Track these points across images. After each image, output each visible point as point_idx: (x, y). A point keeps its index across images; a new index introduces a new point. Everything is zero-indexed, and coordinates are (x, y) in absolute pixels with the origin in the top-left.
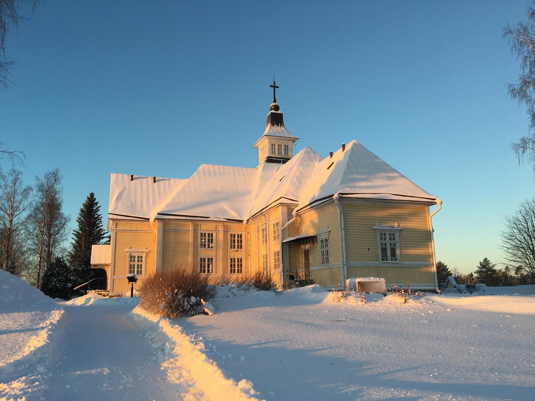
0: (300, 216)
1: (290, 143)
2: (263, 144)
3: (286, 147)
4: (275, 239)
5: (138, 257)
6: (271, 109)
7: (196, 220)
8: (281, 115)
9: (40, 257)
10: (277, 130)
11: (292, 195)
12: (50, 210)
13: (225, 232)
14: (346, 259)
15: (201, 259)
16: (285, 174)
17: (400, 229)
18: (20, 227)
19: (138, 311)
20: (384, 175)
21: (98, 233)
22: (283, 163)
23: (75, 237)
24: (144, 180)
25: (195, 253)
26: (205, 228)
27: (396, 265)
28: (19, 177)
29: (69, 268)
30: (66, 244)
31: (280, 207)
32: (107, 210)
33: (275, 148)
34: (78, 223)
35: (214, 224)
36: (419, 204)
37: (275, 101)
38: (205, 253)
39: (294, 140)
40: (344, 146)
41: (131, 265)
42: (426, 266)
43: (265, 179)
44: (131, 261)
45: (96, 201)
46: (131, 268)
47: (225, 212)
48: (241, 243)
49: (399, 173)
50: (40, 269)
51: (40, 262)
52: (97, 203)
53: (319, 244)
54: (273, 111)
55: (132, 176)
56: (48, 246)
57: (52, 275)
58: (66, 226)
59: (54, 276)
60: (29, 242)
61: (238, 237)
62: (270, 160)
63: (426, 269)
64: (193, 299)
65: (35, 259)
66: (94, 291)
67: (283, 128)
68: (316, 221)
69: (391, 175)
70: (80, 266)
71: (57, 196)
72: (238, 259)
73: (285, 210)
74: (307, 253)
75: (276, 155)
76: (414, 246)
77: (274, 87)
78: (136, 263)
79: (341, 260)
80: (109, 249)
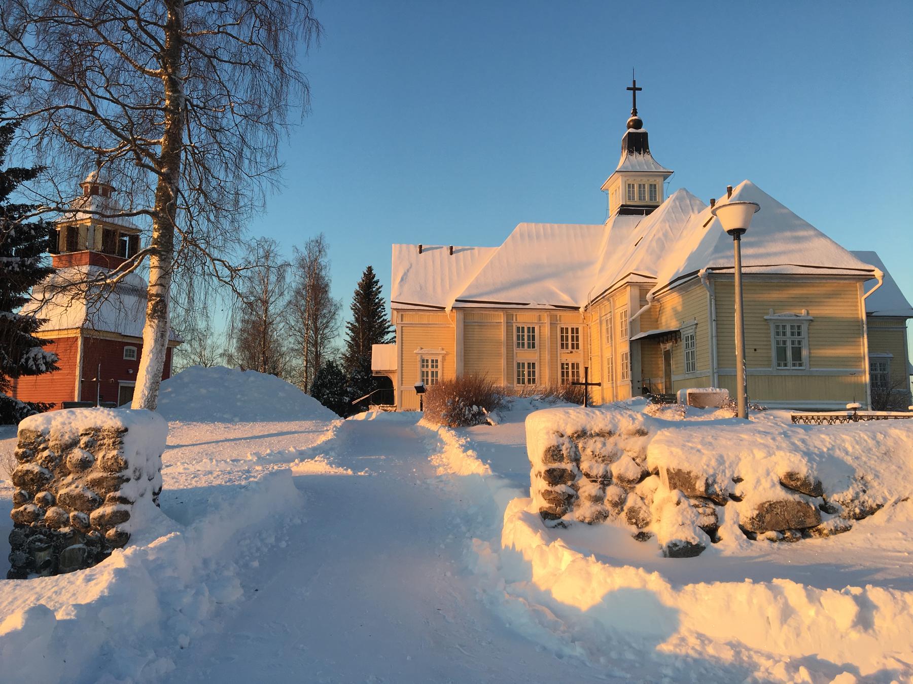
0: (658, 300)
1: (659, 181)
2: (615, 184)
3: (653, 187)
4: (622, 336)
5: (433, 361)
6: (629, 128)
7: (509, 309)
8: (645, 135)
9: (306, 361)
10: (638, 159)
11: (648, 269)
12: (316, 292)
13: (553, 325)
14: (718, 364)
15: (519, 364)
16: (643, 235)
17: (810, 318)
18: (278, 319)
19: (423, 423)
20: (788, 234)
21: (380, 326)
22: (647, 214)
23: (349, 332)
24: (437, 252)
25: (510, 357)
26: (523, 319)
27: (800, 373)
28: (272, 248)
29: (345, 376)
30: (338, 343)
31: (628, 288)
32: (391, 294)
33: (633, 191)
34: (352, 312)
35: (536, 314)
36: (845, 279)
37: (635, 113)
38: (525, 356)
39: (666, 175)
40: (730, 190)
41: (423, 372)
42: (853, 374)
43: (615, 241)
44: (423, 366)
45: (375, 279)
46: (423, 376)
47: (552, 294)
48: (577, 340)
49: (815, 229)
50: (307, 378)
51: (306, 367)
52: (377, 282)
53: (684, 342)
54: (631, 130)
55: (421, 246)
56: (315, 345)
57: (323, 385)
58: (337, 317)
59: (326, 387)
60: (292, 340)
61: (573, 333)
62: (625, 211)
63: (853, 379)
64: (475, 408)
65: (298, 363)
66: (377, 406)
67: (647, 157)
68: (679, 308)
69: (801, 233)
70: (359, 373)
71: (323, 273)
72: (573, 364)
73: (636, 291)
74: (668, 355)
75: (636, 202)
76: (833, 344)
77: (634, 89)
78: (430, 369)
79: (710, 366)
80: (393, 348)
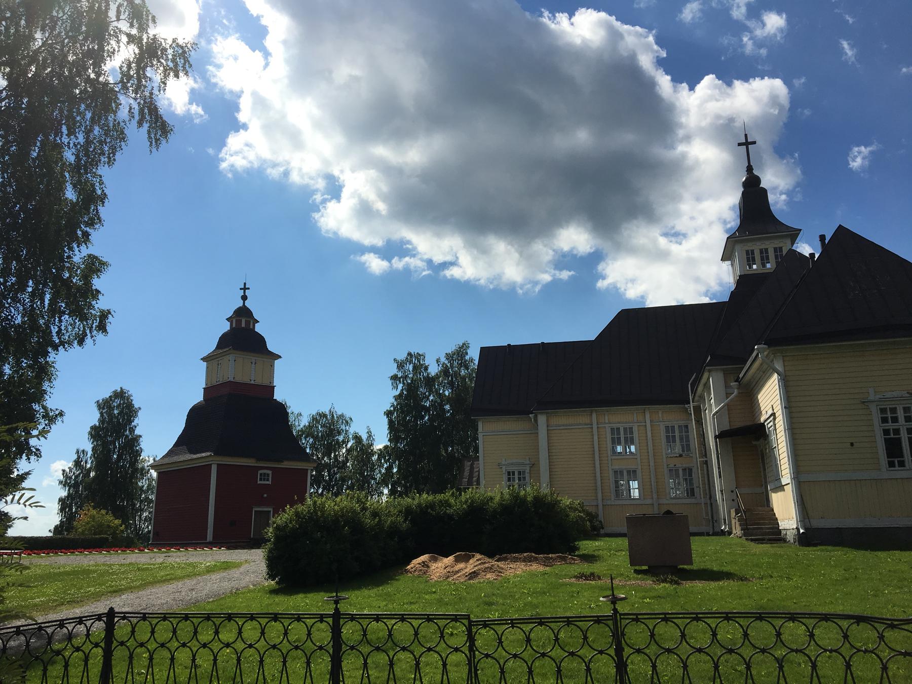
5: (520, 473)
